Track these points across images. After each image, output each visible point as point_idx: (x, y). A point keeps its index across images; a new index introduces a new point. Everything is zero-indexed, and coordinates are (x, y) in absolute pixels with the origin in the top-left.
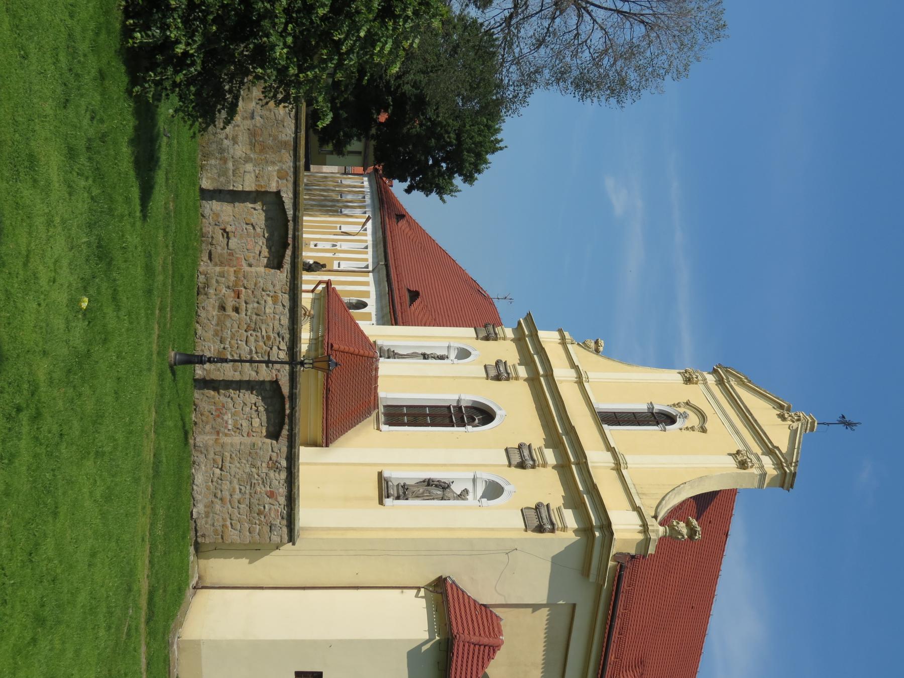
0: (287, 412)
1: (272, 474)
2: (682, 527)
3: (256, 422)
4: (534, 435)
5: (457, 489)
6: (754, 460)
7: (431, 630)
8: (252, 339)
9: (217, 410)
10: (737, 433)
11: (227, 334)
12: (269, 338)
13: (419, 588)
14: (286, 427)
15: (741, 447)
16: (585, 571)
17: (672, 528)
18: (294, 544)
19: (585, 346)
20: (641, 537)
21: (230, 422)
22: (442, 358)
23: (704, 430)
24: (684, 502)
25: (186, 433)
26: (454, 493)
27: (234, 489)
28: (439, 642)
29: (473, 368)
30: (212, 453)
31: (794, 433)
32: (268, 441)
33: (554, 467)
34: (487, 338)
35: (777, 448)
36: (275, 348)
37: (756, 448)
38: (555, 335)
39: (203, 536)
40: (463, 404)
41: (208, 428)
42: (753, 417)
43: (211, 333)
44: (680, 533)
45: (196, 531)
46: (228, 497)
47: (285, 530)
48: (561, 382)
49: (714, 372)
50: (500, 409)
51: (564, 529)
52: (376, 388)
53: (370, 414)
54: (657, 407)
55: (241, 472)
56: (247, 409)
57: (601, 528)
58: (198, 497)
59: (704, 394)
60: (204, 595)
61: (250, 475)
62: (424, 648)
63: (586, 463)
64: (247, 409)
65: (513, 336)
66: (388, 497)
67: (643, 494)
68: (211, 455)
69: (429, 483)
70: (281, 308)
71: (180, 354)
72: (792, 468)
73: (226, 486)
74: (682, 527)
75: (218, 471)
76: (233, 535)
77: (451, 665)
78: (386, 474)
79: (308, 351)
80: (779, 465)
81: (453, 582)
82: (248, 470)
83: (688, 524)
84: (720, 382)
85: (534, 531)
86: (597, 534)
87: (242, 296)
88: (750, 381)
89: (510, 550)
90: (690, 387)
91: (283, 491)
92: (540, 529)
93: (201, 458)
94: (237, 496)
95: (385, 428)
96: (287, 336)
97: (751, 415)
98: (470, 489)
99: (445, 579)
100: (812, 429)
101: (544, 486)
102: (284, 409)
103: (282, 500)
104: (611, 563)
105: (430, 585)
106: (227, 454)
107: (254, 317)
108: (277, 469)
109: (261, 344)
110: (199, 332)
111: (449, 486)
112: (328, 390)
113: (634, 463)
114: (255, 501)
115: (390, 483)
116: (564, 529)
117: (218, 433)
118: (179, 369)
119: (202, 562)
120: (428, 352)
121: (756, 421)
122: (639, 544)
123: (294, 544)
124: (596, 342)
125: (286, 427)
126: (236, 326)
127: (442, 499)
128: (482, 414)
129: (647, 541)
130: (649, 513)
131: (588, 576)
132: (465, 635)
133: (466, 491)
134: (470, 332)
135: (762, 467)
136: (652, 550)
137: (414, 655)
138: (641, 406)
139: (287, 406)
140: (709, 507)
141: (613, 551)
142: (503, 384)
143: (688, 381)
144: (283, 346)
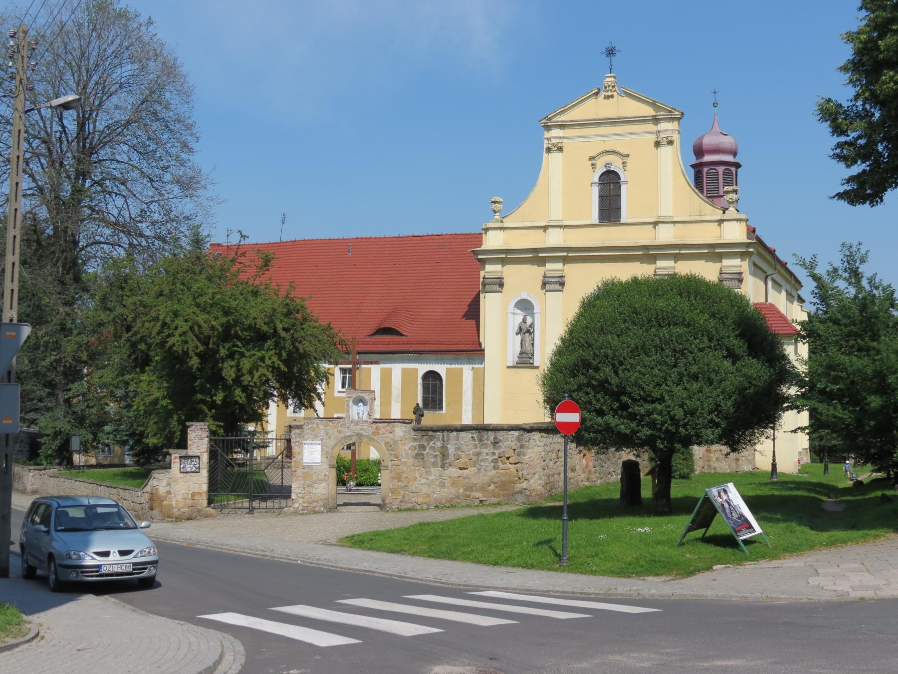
10: (630, 134)
15: (653, 138)
37: (651, 127)
49: (548, 128)
72: (676, 113)
80: (672, 119)
84: (562, 126)
113: (556, 214)
124: (494, 202)
135: (673, 131)
143: (560, 149)
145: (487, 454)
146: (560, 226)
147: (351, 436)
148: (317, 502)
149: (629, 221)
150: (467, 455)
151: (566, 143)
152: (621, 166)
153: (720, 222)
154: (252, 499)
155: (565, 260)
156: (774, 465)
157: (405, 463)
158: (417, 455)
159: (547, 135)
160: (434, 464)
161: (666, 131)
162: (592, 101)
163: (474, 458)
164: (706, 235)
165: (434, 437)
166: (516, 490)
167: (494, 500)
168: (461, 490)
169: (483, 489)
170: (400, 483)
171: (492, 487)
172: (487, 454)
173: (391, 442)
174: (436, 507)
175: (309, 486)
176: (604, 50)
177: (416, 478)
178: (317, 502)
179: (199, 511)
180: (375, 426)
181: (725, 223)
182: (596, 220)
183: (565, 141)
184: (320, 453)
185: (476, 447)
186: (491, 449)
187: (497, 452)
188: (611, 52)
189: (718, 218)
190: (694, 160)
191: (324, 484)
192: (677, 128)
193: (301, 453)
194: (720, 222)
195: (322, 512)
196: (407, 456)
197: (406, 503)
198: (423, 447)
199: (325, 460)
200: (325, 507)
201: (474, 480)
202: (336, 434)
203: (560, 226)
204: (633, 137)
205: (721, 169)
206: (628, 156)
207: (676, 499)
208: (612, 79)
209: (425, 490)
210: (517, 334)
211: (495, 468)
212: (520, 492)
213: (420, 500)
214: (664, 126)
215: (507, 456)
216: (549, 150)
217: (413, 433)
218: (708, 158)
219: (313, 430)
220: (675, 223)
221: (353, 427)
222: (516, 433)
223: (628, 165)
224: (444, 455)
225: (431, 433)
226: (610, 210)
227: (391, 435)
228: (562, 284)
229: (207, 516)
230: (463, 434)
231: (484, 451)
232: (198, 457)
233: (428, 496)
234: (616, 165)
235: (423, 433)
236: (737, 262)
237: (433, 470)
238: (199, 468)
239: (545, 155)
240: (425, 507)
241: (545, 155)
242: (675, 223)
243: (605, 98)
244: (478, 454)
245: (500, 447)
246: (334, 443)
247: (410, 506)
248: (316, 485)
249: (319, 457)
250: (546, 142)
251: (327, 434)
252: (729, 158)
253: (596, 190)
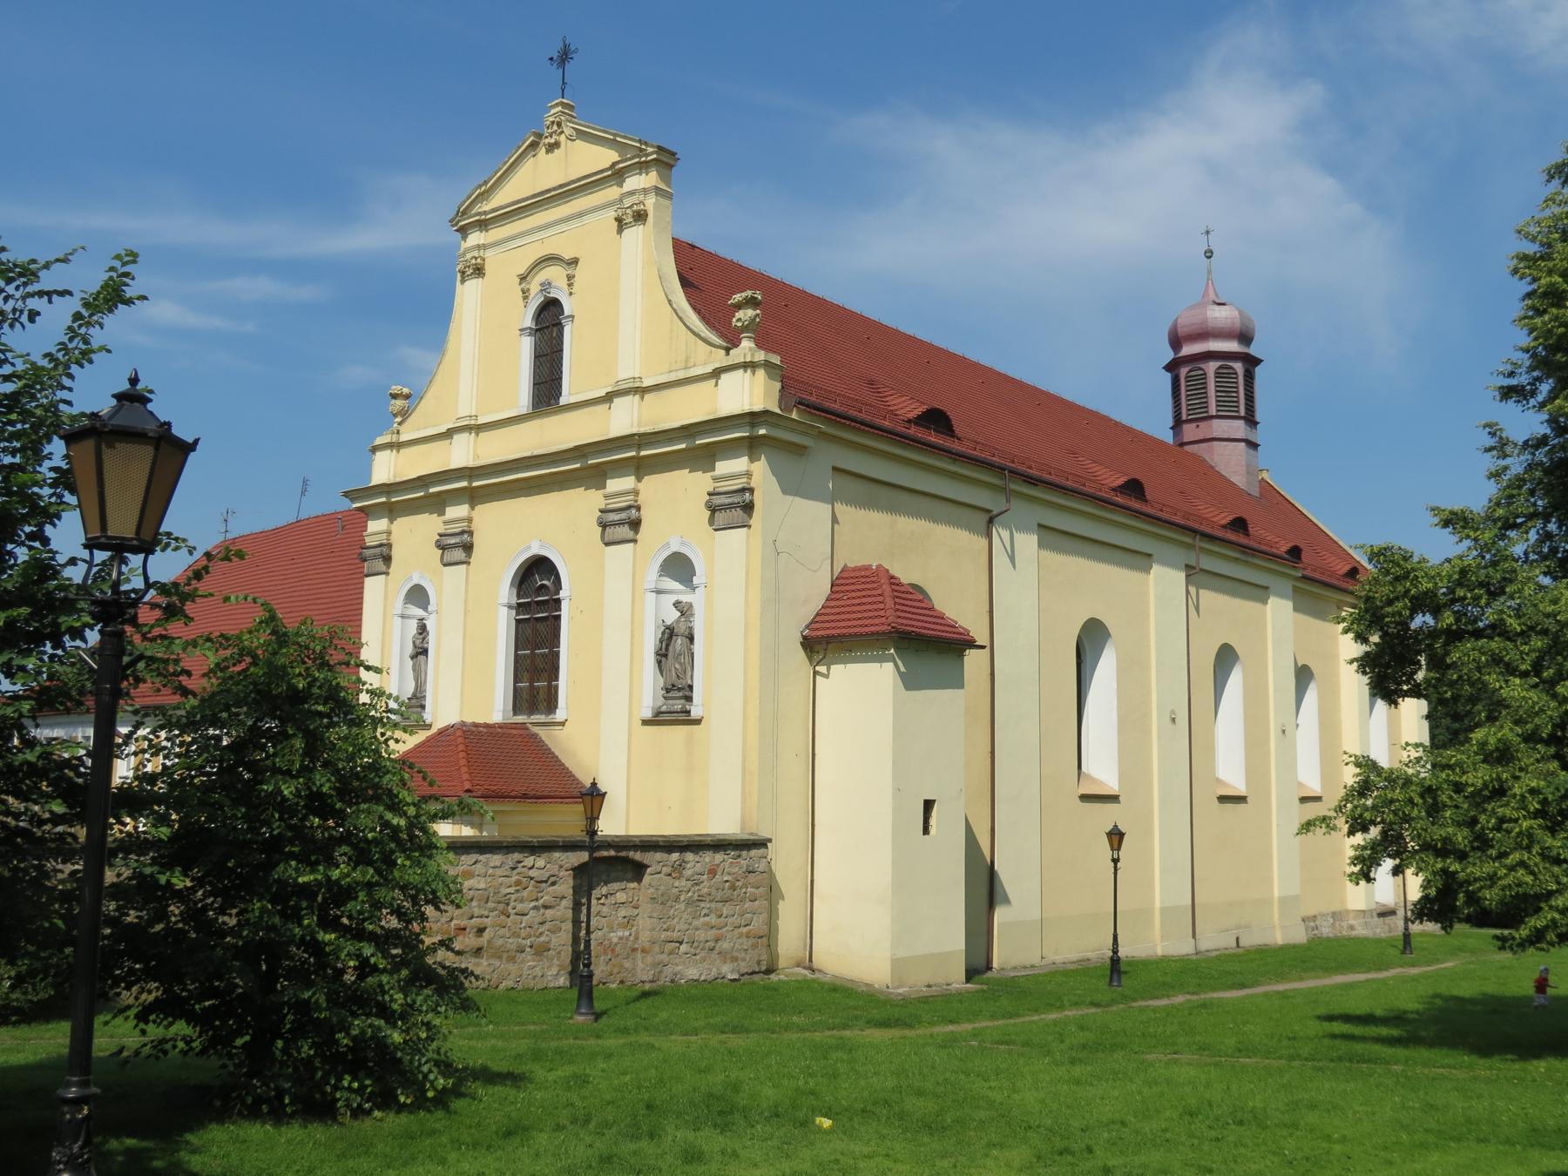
0: (612, 853)
1: (688, 873)
2: (746, 314)
3: (621, 897)
4: (584, 504)
5: (672, 616)
6: (634, 199)
7: (881, 660)
8: (520, 907)
9: (605, 953)
10: (580, 215)
11: (512, 943)
12: (518, 883)
13: (815, 673)
14: (631, 854)
15: (611, 214)
16: (799, 450)
17: (745, 329)
18: (770, 840)
19: (405, 414)
20: (761, 373)
21: (620, 934)
22: (423, 629)
23: (574, 262)
24: (695, 309)
25: (645, 995)
26: (678, 621)
27: (706, 924)
28: (896, 649)
29: (447, 585)
30: (662, 957)
31: (581, 135)
32: (647, 879)
33: (639, 479)
34: (387, 559)
35: (614, 164)
36: (532, 873)
37: (612, 192)
38: (382, 458)
39: (759, 962)
40: (514, 601)
41: (627, 964)
42: (554, 189)
43: (512, 967)
44: (753, 320)
45: (754, 973)
46: (714, 931)
47: (753, 852)
48: (476, 456)
49: (463, 231)
50: (529, 547)
51: (749, 474)
52: (487, 726)
53: (535, 736)
54: (528, 322)
55: (685, 916)
56: (605, 910)
57: (753, 425)
58: (714, 973)
59: (507, 255)
60: (818, 961)
61: (689, 903)
62: (903, 669)
63: (640, 435)
64: (605, 910)
65: (385, 521)
66: (688, 712)
67: (687, 360)
68: (664, 957)
69: (662, 655)
70: (478, 866)
71: (578, 1007)
72: (650, 150)
73: (701, 935)
74: (746, 314)
75: (683, 948)
76: (758, 924)
77: (918, 634)
78: (648, 714)
79: (472, 825)
80: (643, 167)
81: (807, 627)
82: (682, 906)
83: (739, 306)
84: (483, 225)
85: (750, 516)
86: (762, 432)
87: (463, 923)
88: (486, 183)
89: (775, 550)
90: (488, 269)
91: (708, 857)
92: (748, 508)
93: (668, 971)
94: (712, 919)
95: (560, 715)
96: (517, 856)
97: (549, 191)
98: (674, 598)
99: (805, 638)
100: (571, 107)
101: (674, 502)
102: (610, 858)
103: (719, 857)
104: (794, 416)
105: (810, 659)
106: (664, 935)
107: (490, 905)
108: (681, 865)
109: (525, 893)
110: (509, 983)
111: (668, 628)
112: (525, 796)
113: (629, 368)
114: (719, 895)
115: (664, 708)
116: (749, 474)
117: (634, 950)
118: (599, 1005)
119: (782, 963)
120: (410, 649)
121: (561, 186)
122: (770, 376)
123: (770, 840)
124: (394, 396)
125: (631, 854)
126: (502, 931)
127: (691, 639)
128: (537, 580)
129: (767, 365)
130: (719, 359)
131: (805, 447)
132: (888, 618)
133: (677, 604)
134: (373, 587)
135: (645, 191)
136: (776, 359)
137: (910, 682)
138: (527, 345)
139: (605, 853)
140: (706, 280)
141: (778, 411)
142: (478, 541)
143: (479, 271)
144: (529, 861)
149: (573, 400)
156: (1115, 951)
188: (564, 57)
190: (1169, 355)
205: (1212, 367)
207: (99, 1058)
218: (1188, 350)
223: (577, 281)
236: (739, 464)
243: (548, 152)
252: (1232, 346)
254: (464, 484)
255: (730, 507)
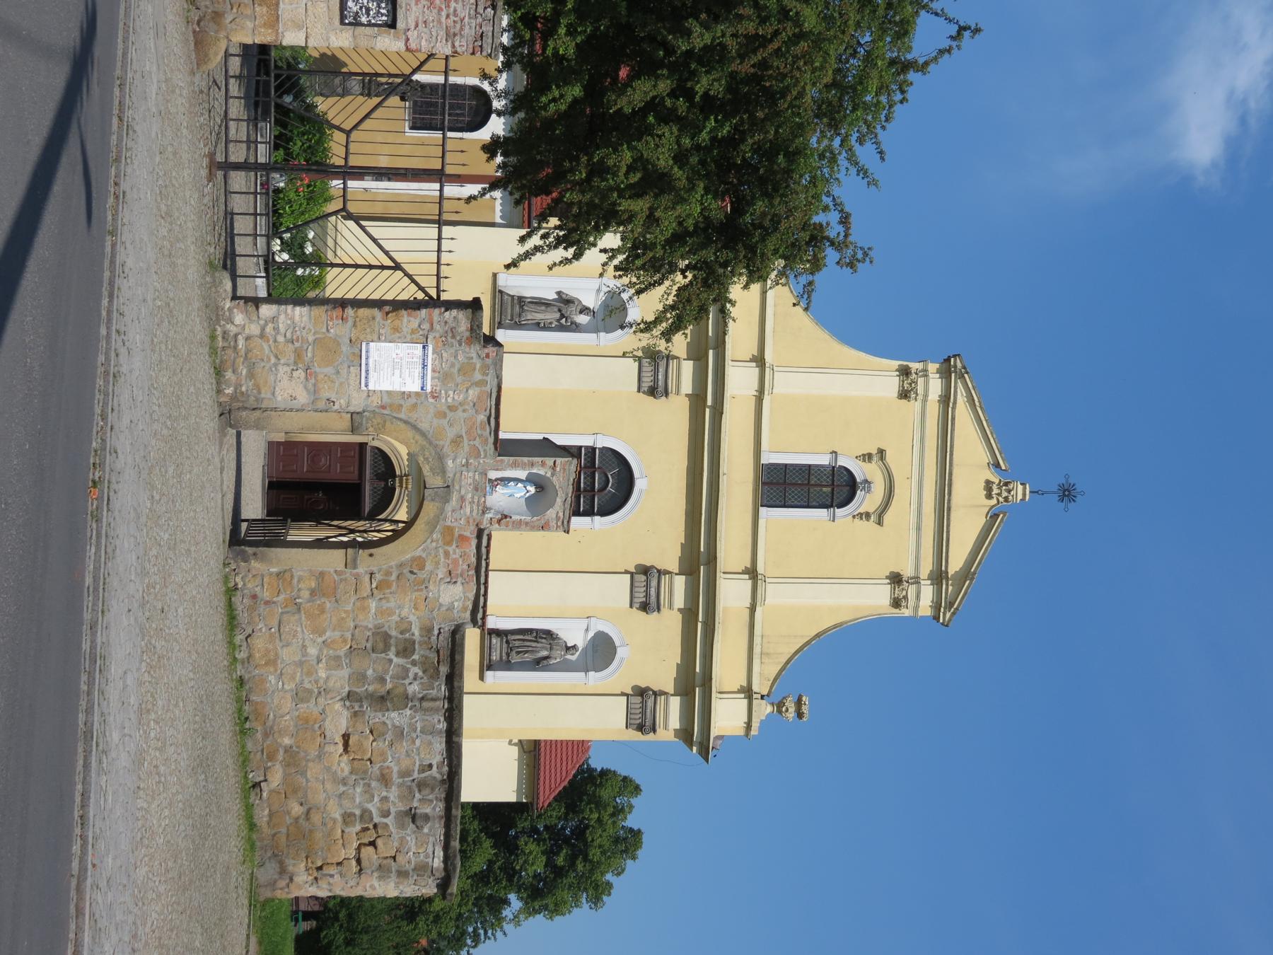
4: (667, 554)
7: (519, 791)
10: (919, 529)
15: (908, 572)
37: (927, 567)
42: (949, 501)
72: (948, 615)
80: (937, 606)
84: (946, 400)
113: (783, 384)
121: (953, 419)
135: (916, 608)
143: (904, 395)
145: (385, 799)
146: (761, 391)
147: (443, 471)
148: (251, 375)
149: (762, 522)
150: (383, 754)
151: (914, 406)
152: (861, 510)
153: (748, 692)
154: (246, 97)
155: (697, 400)
157: (365, 609)
158: (386, 637)
159: (933, 367)
160: (361, 677)
161: (918, 597)
162: (985, 457)
163: (375, 770)
164: (727, 667)
165: (435, 675)
166: (289, 862)
167: (262, 816)
168: (287, 741)
169: (291, 789)
170: (306, 594)
171: (297, 810)
172: (385, 799)
173: (422, 575)
174: (241, 681)
175: (298, 354)
176: (1071, 481)
177: (321, 633)
178: (251, 375)
179: (217, 16)
180: (470, 532)
181: (746, 701)
182: (767, 459)
183: (918, 405)
184: (397, 388)
185: (405, 774)
186: (397, 806)
187: (389, 821)
188: (1067, 493)
189: (755, 688)
191: (303, 398)
192: (920, 613)
193: (396, 336)
194: (748, 692)
195: (219, 392)
196: (381, 612)
197: (252, 609)
198: (406, 649)
199: (375, 401)
200: (234, 397)
201: (314, 770)
202: (451, 433)
203: (761, 391)
204: (913, 533)
206: (880, 523)
208: (1020, 497)
209: (288, 655)
210: (559, 293)
211: (348, 818)
212: (283, 871)
213: (259, 643)
214: (928, 592)
215: (379, 842)
216: (905, 372)
217: (447, 628)
219: (465, 370)
220: (753, 609)
221: (469, 477)
222: (438, 863)
223: (864, 523)
224: (382, 701)
225: (444, 670)
226: (786, 486)
227: (441, 573)
228: (652, 392)
229: (200, 43)
230: (439, 745)
231: (393, 794)
232: (392, 25)
233: (272, 662)
234: (867, 501)
235: (445, 653)
237: (345, 672)
238: (357, 23)
239: (896, 364)
240: (241, 655)
241: (896, 364)
242: (753, 609)
244: (385, 780)
245: (402, 826)
246: (424, 426)
247: (243, 617)
248: (300, 374)
249: (386, 386)
250: (919, 366)
251: (452, 408)
253: (824, 460)
254: (709, 403)
255: (644, 713)
